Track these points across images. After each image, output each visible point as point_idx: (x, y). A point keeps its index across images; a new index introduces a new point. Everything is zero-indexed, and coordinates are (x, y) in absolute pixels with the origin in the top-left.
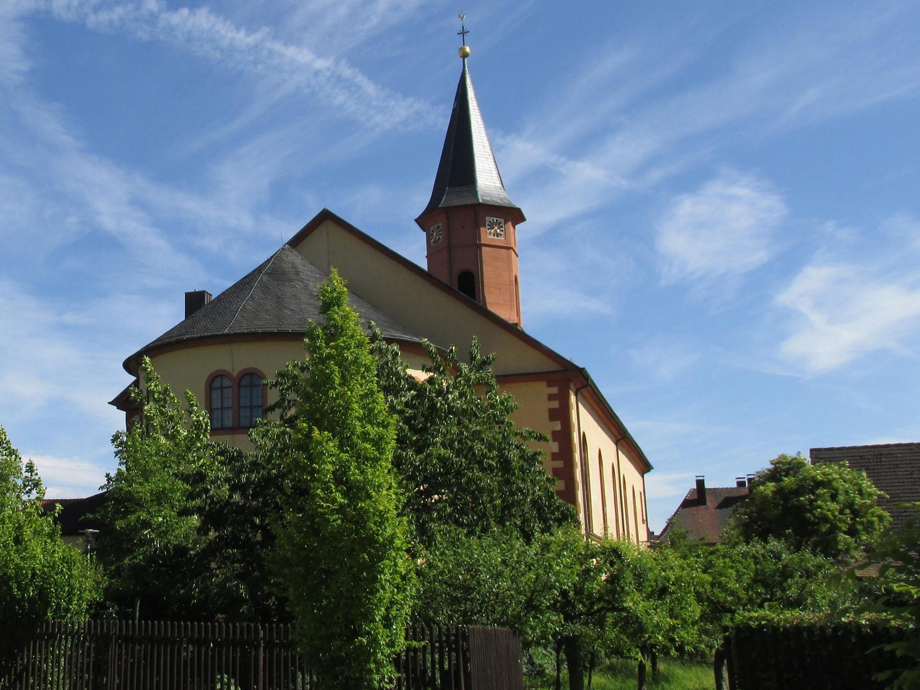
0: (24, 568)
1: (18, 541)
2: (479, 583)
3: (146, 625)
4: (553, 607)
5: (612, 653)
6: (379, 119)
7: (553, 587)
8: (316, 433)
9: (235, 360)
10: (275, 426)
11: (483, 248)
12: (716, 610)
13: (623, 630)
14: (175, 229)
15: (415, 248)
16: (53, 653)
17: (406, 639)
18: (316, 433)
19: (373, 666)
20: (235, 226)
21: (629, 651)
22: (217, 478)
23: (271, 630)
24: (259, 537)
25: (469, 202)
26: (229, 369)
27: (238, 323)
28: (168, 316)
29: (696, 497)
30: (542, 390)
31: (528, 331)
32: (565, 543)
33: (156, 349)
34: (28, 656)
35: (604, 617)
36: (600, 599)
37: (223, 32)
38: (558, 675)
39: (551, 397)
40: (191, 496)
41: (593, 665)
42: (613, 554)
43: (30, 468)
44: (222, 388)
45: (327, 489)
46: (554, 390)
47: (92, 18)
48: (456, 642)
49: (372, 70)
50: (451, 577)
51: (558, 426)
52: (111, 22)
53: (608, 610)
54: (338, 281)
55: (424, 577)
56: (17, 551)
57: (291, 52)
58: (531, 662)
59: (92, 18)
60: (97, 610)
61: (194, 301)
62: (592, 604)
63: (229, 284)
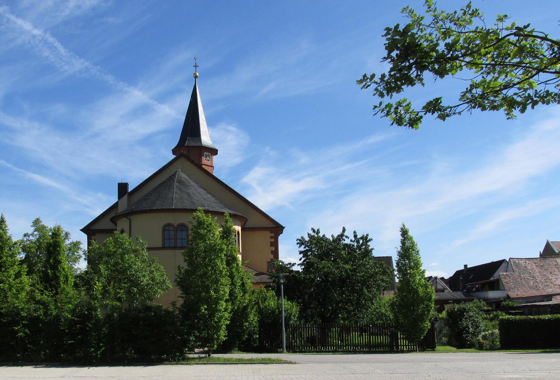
6: (66, 67)
25: (198, 145)
26: (172, 222)
30: (268, 234)
39: (271, 237)
44: (169, 230)
46: (273, 235)
49: (64, 39)
51: (273, 249)
57: (20, 22)
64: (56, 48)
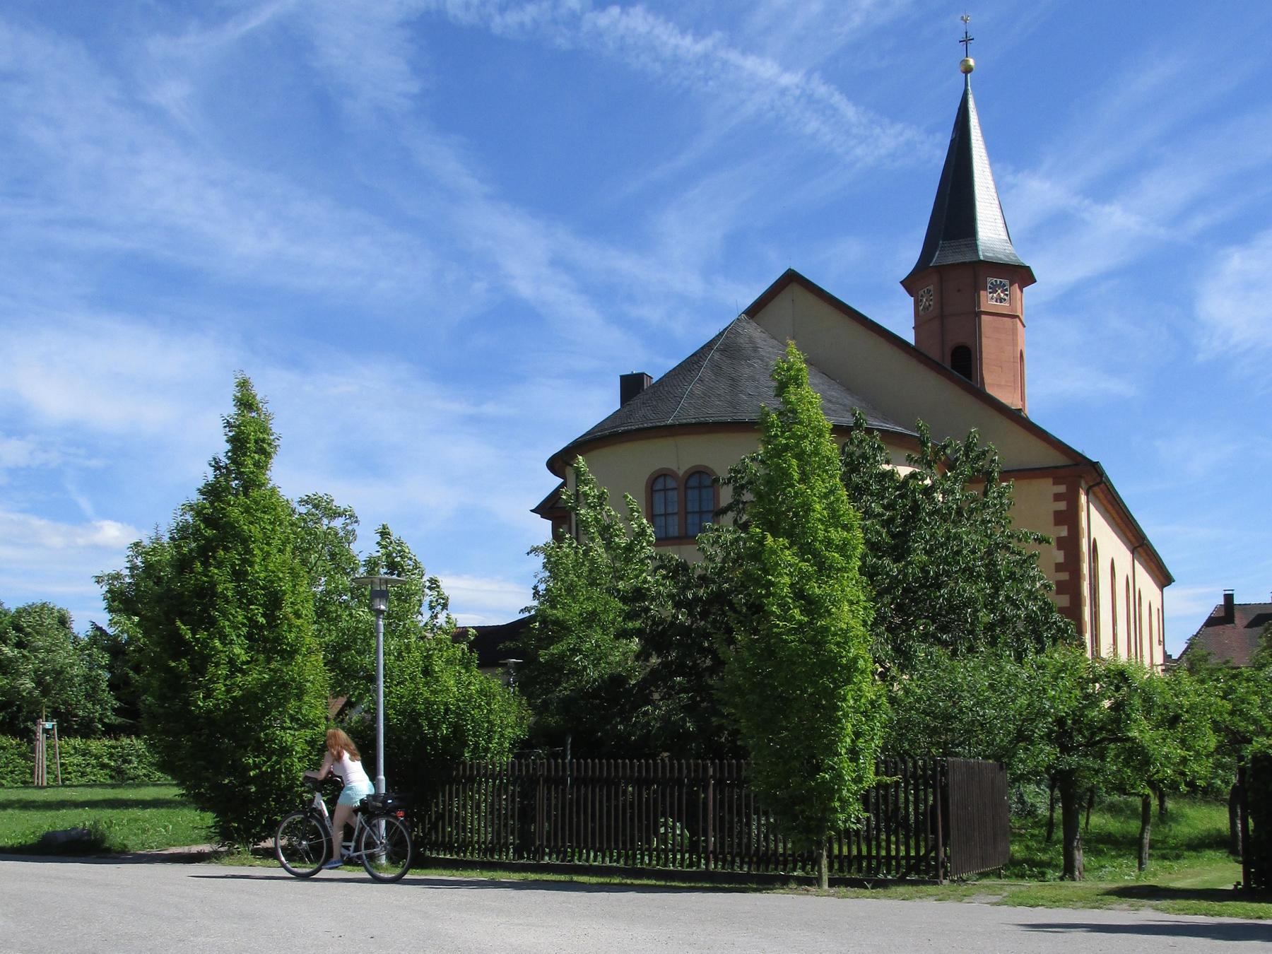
0: (435, 702)
1: (427, 672)
2: (961, 710)
3: (579, 763)
4: (1048, 737)
5: (1113, 789)
6: (859, 151)
7: (1047, 714)
8: (770, 540)
9: (681, 456)
10: (728, 531)
11: (983, 317)
12: (1234, 740)
13: (1127, 763)
14: (607, 295)
15: (899, 317)
16: (472, 798)
17: (877, 774)
18: (770, 540)
19: (837, 804)
20: (678, 290)
21: (1132, 787)
22: (659, 593)
23: (722, 765)
24: (708, 662)
26: (674, 467)
27: (684, 412)
28: (600, 404)
29: (1222, 614)
31: (1034, 419)
32: (1064, 664)
33: (586, 444)
34: (444, 802)
35: (1106, 748)
36: (1101, 729)
37: (665, 38)
38: (1051, 816)
39: (1057, 497)
40: (629, 616)
41: (1091, 804)
42: (1120, 677)
43: (434, 584)
44: (665, 490)
45: (784, 606)
46: (1062, 489)
47: (498, 19)
48: (933, 777)
49: (853, 86)
50: (930, 705)
52: (522, 25)
53: (1111, 741)
54: (796, 358)
55: (899, 705)
56: (427, 684)
57: (750, 63)
58: (1021, 800)
59: (498, 19)
60: (522, 748)
61: (632, 385)
62: (1093, 734)
63: (674, 363)
64: (836, 110)
